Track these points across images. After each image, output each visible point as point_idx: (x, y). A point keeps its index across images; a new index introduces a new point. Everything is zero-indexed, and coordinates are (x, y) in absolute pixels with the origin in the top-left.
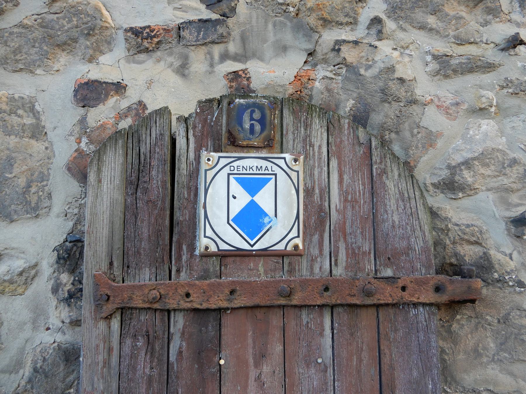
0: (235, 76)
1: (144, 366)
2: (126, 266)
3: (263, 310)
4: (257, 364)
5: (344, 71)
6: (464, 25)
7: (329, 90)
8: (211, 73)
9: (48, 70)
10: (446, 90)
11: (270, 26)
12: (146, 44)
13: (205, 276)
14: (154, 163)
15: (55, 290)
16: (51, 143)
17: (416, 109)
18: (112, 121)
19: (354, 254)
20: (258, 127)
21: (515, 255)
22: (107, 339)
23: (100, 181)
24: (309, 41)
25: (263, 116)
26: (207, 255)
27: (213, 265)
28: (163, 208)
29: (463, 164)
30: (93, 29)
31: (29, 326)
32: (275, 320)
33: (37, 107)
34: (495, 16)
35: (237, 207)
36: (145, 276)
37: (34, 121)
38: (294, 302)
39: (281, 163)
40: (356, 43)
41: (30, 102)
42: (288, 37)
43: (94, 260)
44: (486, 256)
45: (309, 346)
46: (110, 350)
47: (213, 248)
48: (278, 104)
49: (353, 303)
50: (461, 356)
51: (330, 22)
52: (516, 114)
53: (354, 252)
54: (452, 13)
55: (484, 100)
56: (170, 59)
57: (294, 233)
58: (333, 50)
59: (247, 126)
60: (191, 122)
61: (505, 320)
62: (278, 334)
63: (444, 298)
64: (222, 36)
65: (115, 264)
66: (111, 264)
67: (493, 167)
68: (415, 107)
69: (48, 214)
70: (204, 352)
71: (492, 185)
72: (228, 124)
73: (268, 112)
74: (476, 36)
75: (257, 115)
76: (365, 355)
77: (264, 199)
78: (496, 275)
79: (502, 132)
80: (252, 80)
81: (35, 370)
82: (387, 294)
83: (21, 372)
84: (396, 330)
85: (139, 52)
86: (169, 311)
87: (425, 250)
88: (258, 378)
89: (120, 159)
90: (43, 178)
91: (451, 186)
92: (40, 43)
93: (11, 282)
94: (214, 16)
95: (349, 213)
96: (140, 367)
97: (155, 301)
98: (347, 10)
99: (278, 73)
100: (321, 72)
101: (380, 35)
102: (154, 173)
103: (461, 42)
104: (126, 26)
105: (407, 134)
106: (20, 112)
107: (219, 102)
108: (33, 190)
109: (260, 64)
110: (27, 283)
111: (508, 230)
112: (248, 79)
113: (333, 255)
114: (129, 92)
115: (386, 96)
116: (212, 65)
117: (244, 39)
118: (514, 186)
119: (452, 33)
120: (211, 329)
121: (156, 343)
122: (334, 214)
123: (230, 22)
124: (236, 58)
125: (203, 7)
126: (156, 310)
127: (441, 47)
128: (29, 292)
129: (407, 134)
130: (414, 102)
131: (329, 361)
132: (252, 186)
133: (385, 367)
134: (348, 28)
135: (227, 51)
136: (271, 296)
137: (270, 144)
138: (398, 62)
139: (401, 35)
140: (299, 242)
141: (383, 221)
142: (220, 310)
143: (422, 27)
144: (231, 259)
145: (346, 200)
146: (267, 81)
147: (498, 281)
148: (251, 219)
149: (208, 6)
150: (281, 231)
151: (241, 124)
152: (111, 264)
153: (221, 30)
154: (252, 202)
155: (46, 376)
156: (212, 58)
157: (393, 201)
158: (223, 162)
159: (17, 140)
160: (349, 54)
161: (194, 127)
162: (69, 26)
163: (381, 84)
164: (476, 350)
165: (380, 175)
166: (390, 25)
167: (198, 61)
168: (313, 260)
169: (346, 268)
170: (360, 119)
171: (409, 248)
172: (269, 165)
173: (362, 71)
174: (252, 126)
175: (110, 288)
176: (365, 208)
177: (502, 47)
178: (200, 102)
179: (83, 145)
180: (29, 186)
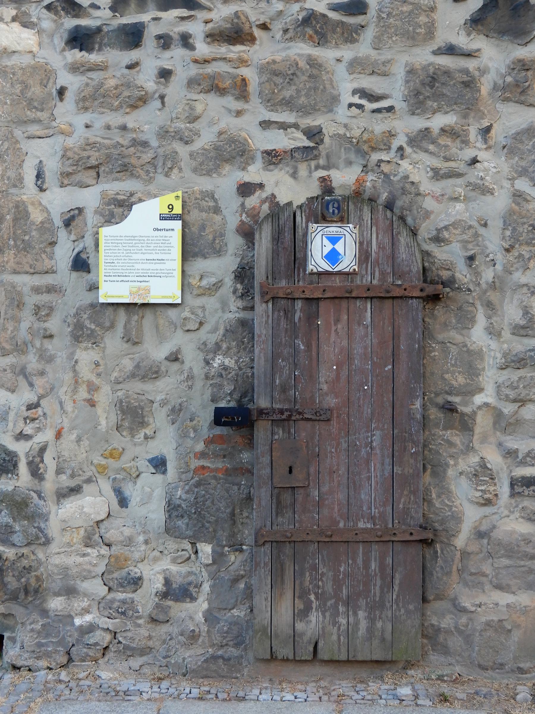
0: (323, 180)
1: (283, 324)
2: (274, 279)
3: (339, 300)
4: (335, 324)
5: (382, 176)
6: (450, 149)
7: (374, 187)
8: (310, 176)
9: (219, 175)
10: (437, 188)
11: (343, 150)
12: (274, 160)
13: (311, 283)
14: (286, 229)
15: (234, 292)
16: (224, 216)
17: (419, 198)
18: (258, 205)
19: (383, 274)
20: (336, 211)
21: (468, 276)
22: (267, 312)
23: (261, 238)
24: (364, 159)
25: (339, 205)
26: (312, 273)
27: (315, 278)
28: (293, 253)
29: (444, 228)
30: (244, 152)
31: (220, 311)
32: (344, 303)
33: (216, 196)
34: (466, 145)
35: (326, 251)
36: (283, 283)
37: (214, 204)
38: (353, 295)
39: (348, 229)
40: (389, 162)
41: (212, 193)
42: (352, 156)
43: (260, 273)
44: (453, 276)
45: (360, 316)
46: (268, 316)
47: (315, 270)
48: (346, 199)
49: (380, 297)
50: (438, 326)
51: (376, 149)
52: (475, 200)
53: (383, 273)
54: (443, 143)
55: (456, 193)
56: (287, 169)
57: (353, 263)
58: (377, 165)
59: (331, 211)
60: (303, 209)
61: (460, 308)
62: (345, 311)
63: (424, 294)
64: (316, 156)
65: (269, 278)
66: (267, 277)
67: (459, 230)
68: (419, 197)
69: (225, 254)
70: (311, 318)
71: (459, 239)
72: (321, 210)
73: (341, 204)
74: (455, 156)
75: (336, 205)
76: (386, 321)
77: (339, 247)
78: (457, 286)
79: (467, 210)
80: (333, 181)
81: (227, 330)
82: (397, 292)
83: (218, 333)
84: (402, 310)
85: (270, 164)
86: (294, 299)
87: (418, 272)
88: (336, 330)
89: (270, 228)
90: (222, 235)
91: (438, 239)
92: (215, 160)
93: (209, 289)
94: (312, 144)
95: (381, 254)
96: (282, 324)
97: (289, 294)
98: (385, 141)
99: (347, 178)
100: (371, 177)
101: (402, 157)
102: (286, 234)
103: (447, 159)
104: (262, 149)
105: (415, 212)
106: (207, 199)
107: (317, 198)
108: (217, 241)
109: (337, 171)
110: (217, 290)
111: (466, 262)
112: (331, 181)
113: (373, 274)
114: (266, 188)
115: (404, 191)
116: (310, 172)
117: (328, 157)
118: (470, 240)
119: (442, 155)
120: (314, 307)
121: (288, 313)
122: (373, 253)
123: (321, 147)
124: (324, 168)
125: (305, 138)
126: (288, 299)
127: (436, 163)
128: (217, 295)
129: (415, 212)
130: (418, 194)
131: (369, 324)
132: (334, 240)
133: (396, 327)
134: (385, 152)
135: (318, 164)
136: (342, 292)
137: (343, 220)
138: (411, 173)
139: (414, 156)
140: (356, 267)
141: (398, 258)
142: (318, 299)
143: (426, 151)
144: (323, 276)
145: (379, 247)
146: (341, 183)
147: (458, 288)
148: (333, 257)
149: (308, 138)
150: (348, 262)
151: (328, 209)
152: (267, 277)
153: (315, 152)
154: (334, 249)
155: (233, 333)
156: (310, 168)
157: (403, 248)
158: (319, 229)
159: (207, 214)
160: (385, 168)
161: (305, 212)
162: (230, 149)
163: (402, 185)
164: (445, 323)
165: (397, 235)
166: (408, 150)
167: (303, 169)
168: (362, 277)
169: (379, 280)
170: (389, 206)
171: (410, 271)
172: (342, 230)
173: (392, 178)
174: (333, 211)
175: (268, 288)
176: (389, 251)
177: (469, 163)
178: (307, 198)
179: (243, 218)
180: (214, 240)
